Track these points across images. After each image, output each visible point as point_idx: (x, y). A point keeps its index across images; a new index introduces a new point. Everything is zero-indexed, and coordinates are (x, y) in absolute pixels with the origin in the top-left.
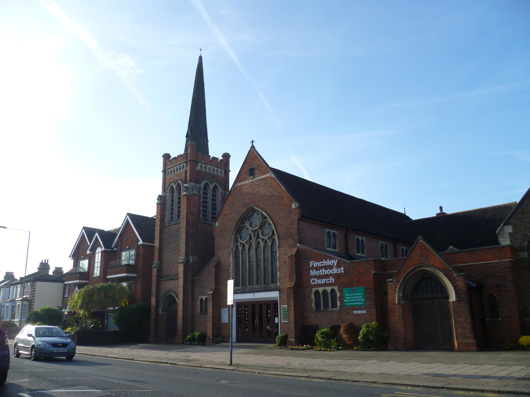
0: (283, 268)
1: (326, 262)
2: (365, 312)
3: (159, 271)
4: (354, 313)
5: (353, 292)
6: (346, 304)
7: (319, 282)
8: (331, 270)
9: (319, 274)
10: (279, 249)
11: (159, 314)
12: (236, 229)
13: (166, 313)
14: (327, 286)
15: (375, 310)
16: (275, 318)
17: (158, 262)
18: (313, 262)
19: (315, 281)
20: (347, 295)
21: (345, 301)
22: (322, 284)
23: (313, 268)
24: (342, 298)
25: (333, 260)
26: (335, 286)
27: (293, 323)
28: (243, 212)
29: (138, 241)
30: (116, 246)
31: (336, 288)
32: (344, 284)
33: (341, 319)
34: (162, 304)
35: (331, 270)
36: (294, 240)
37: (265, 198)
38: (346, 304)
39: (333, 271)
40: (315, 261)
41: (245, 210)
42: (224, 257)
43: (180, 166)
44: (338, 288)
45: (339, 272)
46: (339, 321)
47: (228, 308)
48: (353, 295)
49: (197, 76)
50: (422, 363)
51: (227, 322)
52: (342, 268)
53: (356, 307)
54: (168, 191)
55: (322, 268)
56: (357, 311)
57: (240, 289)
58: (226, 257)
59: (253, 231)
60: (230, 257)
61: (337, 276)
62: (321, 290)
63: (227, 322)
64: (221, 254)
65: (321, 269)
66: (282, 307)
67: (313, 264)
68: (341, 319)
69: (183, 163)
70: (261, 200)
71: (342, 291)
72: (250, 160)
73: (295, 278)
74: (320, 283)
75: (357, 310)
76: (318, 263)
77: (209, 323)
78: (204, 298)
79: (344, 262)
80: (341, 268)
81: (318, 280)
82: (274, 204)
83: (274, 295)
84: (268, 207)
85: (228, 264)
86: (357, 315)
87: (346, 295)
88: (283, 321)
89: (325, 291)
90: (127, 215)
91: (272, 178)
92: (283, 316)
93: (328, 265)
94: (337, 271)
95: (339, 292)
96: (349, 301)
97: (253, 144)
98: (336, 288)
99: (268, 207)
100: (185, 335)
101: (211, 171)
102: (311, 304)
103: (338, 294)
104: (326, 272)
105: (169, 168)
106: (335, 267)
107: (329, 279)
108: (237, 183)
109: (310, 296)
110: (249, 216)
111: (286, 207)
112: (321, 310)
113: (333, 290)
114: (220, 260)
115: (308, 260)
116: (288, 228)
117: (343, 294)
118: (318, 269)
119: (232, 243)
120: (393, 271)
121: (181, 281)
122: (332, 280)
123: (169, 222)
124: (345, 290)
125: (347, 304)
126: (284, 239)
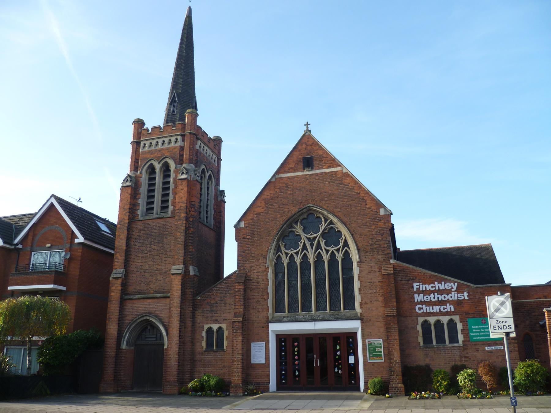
0: (367, 290)
1: (440, 285)
2: (486, 347)
3: (125, 285)
4: (486, 349)
5: (483, 323)
6: (474, 338)
7: (430, 309)
8: (448, 295)
9: (429, 300)
10: (360, 264)
11: (122, 349)
12: (279, 233)
13: (132, 348)
14: (442, 315)
15: (516, 345)
16: (349, 356)
17: (124, 270)
18: (418, 284)
19: (422, 308)
20: (474, 327)
21: (471, 334)
22: (434, 312)
23: (419, 292)
24: (465, 331)
25: (450, 282)
26: (454, 315)
27: (397, 363)
28: (293, 212)
29: (74, 236)
30: (22, 241)
31: (457, 318)
32: (470, 314)
33: (465, 357)
34: (128, 334)
35: (448, 295)
36: (385, 254)
37: (333, 198)
38: (474, 338)
39: (451, 297)
40: (421, 284)
41: (296, 209)
42: (256, 270)
43: (163, 139)
44: (460, 318)
45: (461, 298)
46: (463, 359)
47: (264, 343)
48: (483, 327)
49: (186, 31)
50: (312, 410)
51: (263, 362)
52: (466, 294)
53: (489, 342)
54: (144, 171)
55: (433, 292)
56: (490, 347)
57: (287, 316)
58: (260, 270)
59: (309, 239)
60: (268, 272)
61: (458, 303)
62: (432, 320)
63: (263, 362)
64: (251, 267)
65: (432, 294)
66: (368, 341)
67: (418, 287)
68: (465, 357)
69: (176, 135)
70: (326, 199)
71: (467, 322)
72: (304, 146)
73: (395, 303)
74: (432, 311)
75: (489, 345)
76: (427, 286)
77: (237, 363)
78: (215, 327)
79: (468, 286)
80: (463, 293)
81: (428, 307)
82: (349, 206)
83: (354, 325)
84: (339, 210)
85: (265, 280)
86: (491, 352)
87: (473, 327)
88: (370, 360)
89: (438, 324)
90: (51, 197)
91: (345, 173)
92: (369, 354)
93: (444, 288)
94: (458, 297)
95: (461, 323)
96: (478, 334)
97: (308, 128)
98: (457, 318)
99: (339, 210)
100: (182, 382)
101: (208, 155)
102: (417, 337)
103: (460, 326)
104: (441, 298)
105: (167, 137)
106: (455, 291)
107: (445, 307)
108: (281, 173)
109: (414, 328)
110: (301, 218)
111: (369, 212)
112: (434, 346)
113: (451, 321)
114: (249, 274)
115: (410, 282)
116: (373, 238)
117: (467, 325)
118: (426, 293)
119: (272, 251)
120: (524, 301)
121: (176, 301)
122: (450, 308)
123: (144, 214)
124: (470, 321)
125: (476, 338)
126: (367, 252)
